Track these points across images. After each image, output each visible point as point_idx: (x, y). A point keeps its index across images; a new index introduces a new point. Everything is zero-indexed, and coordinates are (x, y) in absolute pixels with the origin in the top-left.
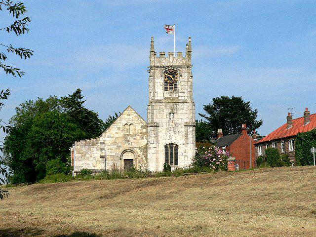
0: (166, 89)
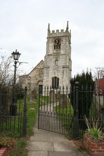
0: (55, 49)
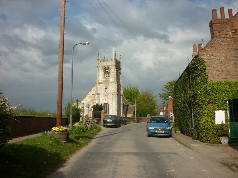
0: (104, 77)
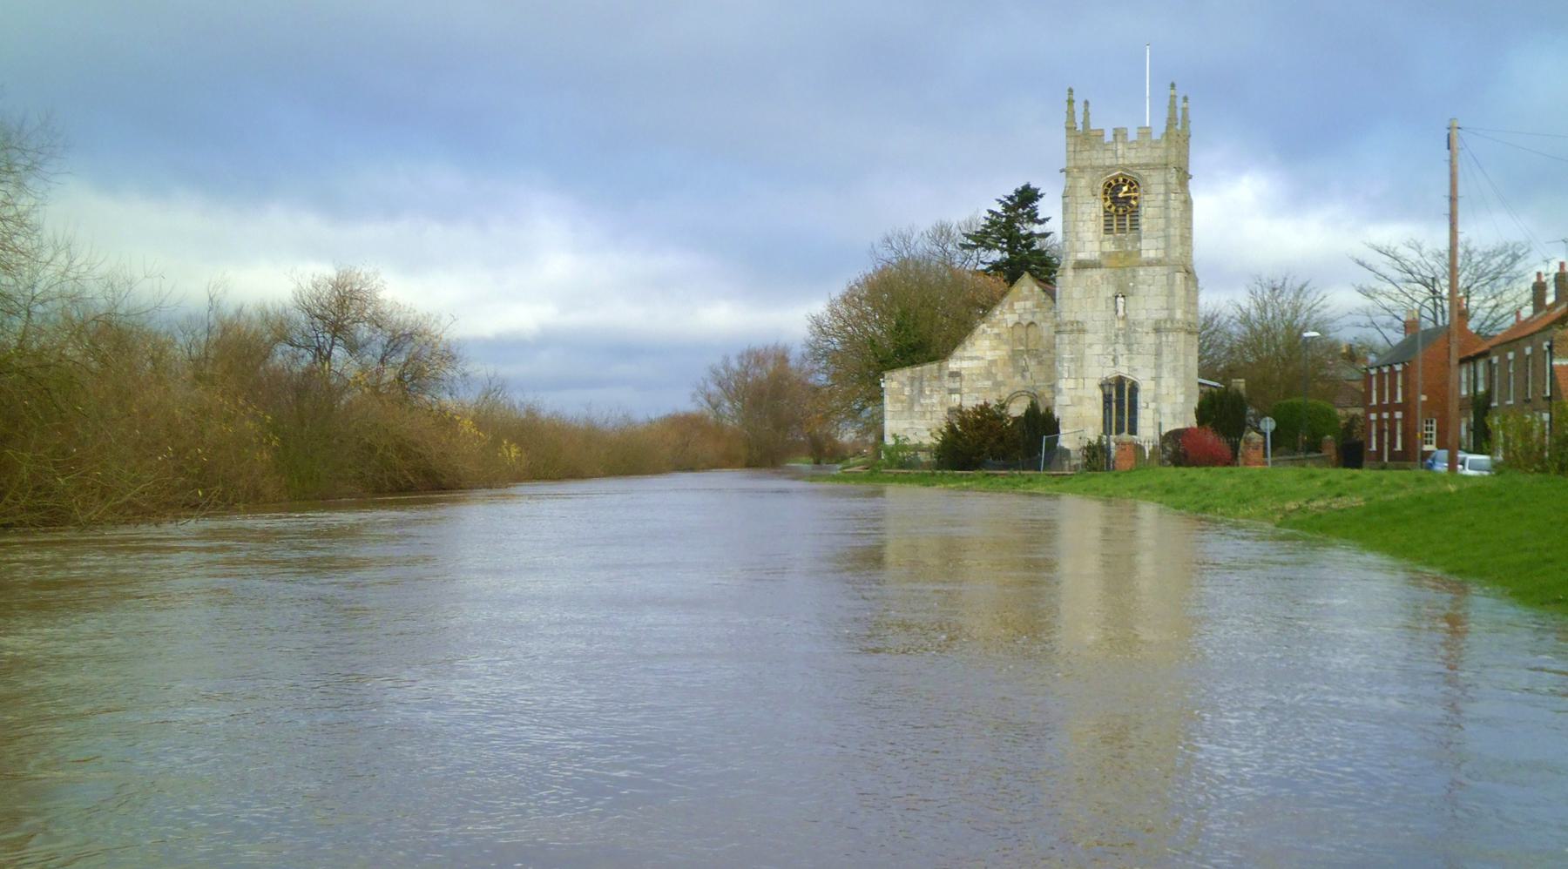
0: (1108, 230)
